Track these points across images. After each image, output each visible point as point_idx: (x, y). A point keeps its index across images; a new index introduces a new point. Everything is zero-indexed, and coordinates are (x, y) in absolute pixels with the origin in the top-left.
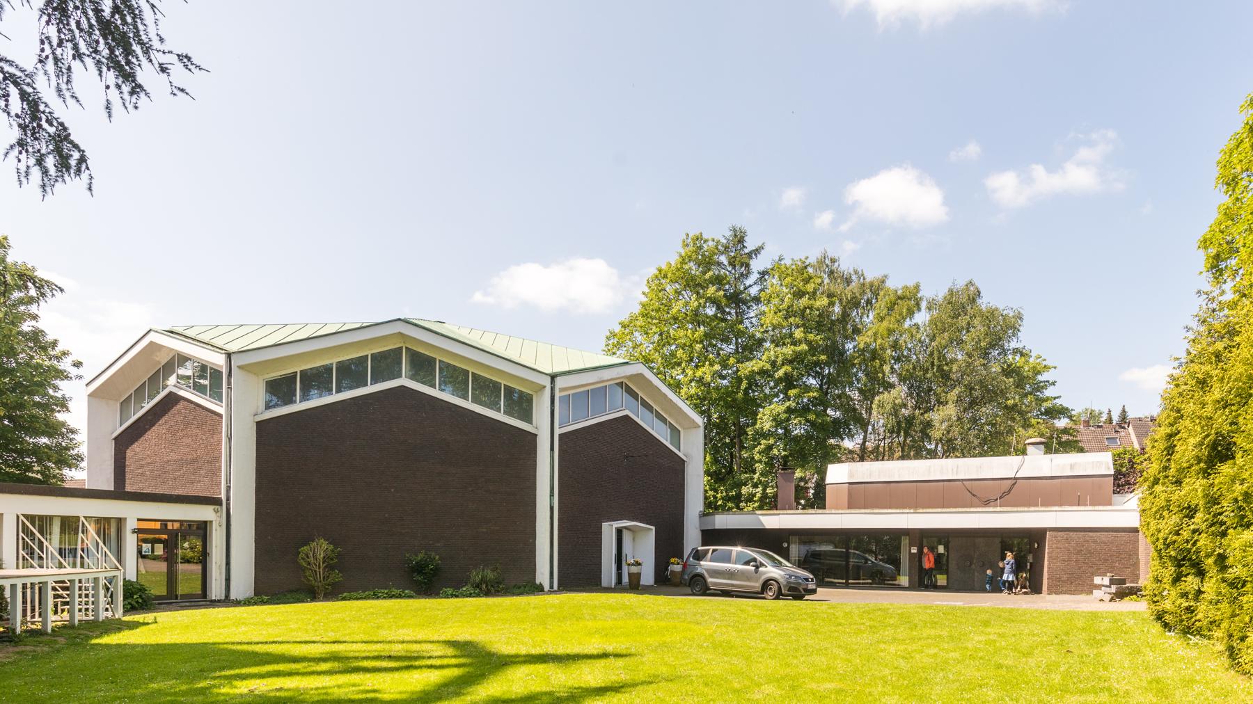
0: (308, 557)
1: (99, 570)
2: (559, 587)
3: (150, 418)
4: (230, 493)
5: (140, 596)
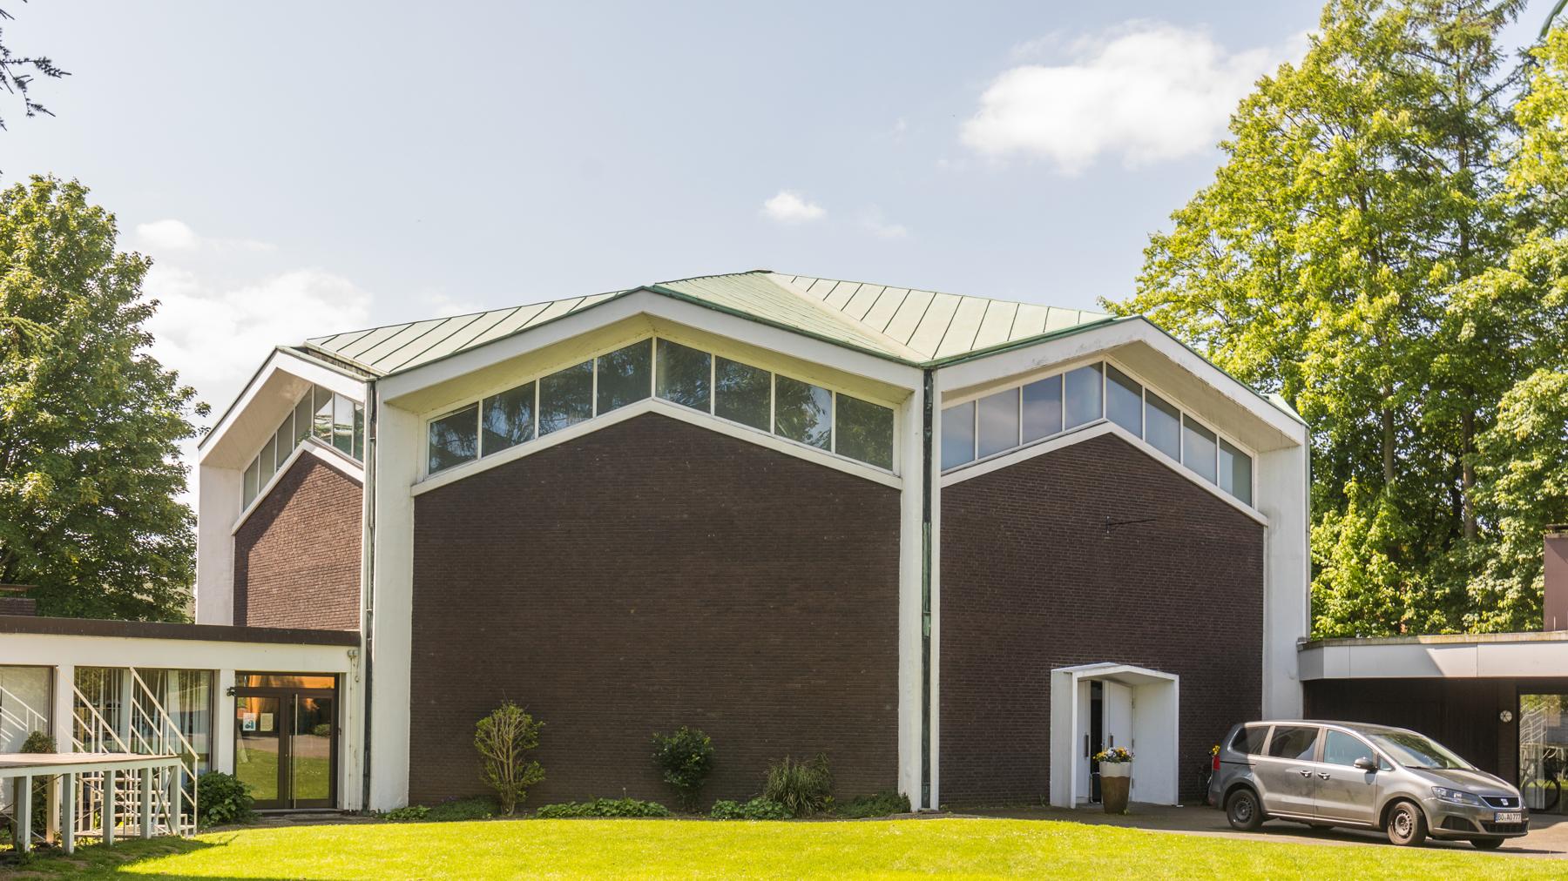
0: (489, 737)
1: (161, 756)
2: (942, 800)
3: (278, 496)
4: (371, 624)
5: (234, 800)
